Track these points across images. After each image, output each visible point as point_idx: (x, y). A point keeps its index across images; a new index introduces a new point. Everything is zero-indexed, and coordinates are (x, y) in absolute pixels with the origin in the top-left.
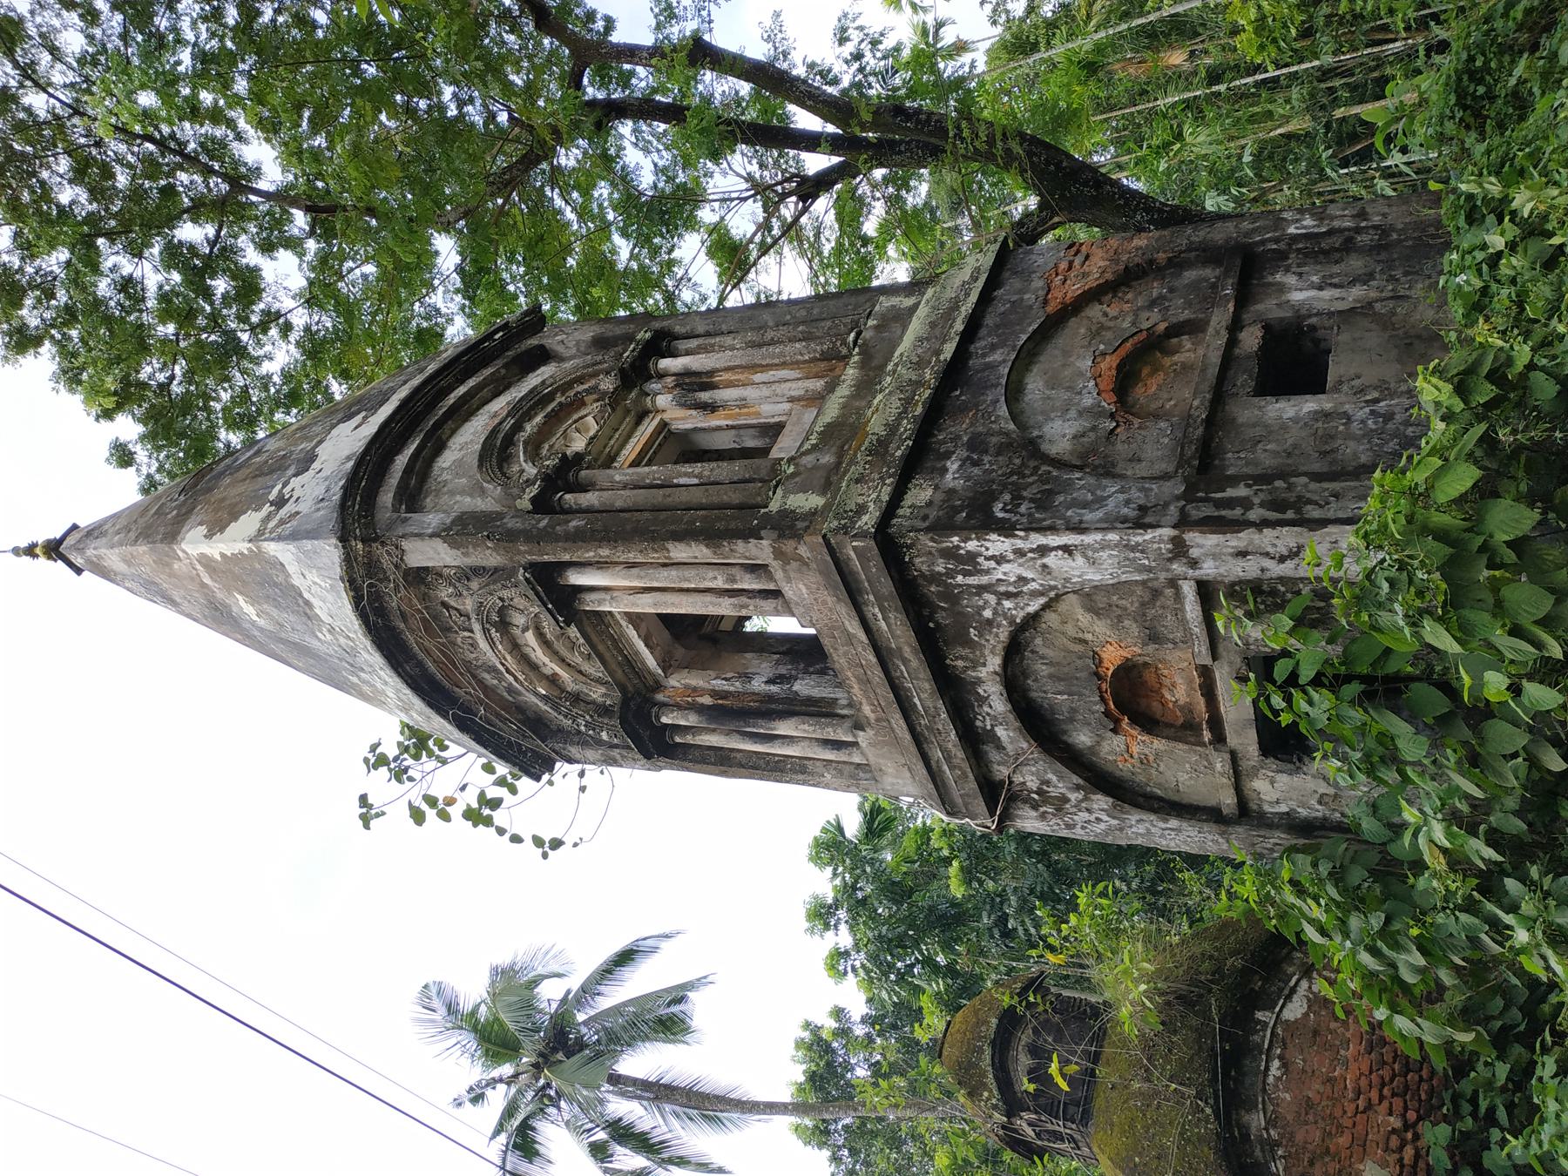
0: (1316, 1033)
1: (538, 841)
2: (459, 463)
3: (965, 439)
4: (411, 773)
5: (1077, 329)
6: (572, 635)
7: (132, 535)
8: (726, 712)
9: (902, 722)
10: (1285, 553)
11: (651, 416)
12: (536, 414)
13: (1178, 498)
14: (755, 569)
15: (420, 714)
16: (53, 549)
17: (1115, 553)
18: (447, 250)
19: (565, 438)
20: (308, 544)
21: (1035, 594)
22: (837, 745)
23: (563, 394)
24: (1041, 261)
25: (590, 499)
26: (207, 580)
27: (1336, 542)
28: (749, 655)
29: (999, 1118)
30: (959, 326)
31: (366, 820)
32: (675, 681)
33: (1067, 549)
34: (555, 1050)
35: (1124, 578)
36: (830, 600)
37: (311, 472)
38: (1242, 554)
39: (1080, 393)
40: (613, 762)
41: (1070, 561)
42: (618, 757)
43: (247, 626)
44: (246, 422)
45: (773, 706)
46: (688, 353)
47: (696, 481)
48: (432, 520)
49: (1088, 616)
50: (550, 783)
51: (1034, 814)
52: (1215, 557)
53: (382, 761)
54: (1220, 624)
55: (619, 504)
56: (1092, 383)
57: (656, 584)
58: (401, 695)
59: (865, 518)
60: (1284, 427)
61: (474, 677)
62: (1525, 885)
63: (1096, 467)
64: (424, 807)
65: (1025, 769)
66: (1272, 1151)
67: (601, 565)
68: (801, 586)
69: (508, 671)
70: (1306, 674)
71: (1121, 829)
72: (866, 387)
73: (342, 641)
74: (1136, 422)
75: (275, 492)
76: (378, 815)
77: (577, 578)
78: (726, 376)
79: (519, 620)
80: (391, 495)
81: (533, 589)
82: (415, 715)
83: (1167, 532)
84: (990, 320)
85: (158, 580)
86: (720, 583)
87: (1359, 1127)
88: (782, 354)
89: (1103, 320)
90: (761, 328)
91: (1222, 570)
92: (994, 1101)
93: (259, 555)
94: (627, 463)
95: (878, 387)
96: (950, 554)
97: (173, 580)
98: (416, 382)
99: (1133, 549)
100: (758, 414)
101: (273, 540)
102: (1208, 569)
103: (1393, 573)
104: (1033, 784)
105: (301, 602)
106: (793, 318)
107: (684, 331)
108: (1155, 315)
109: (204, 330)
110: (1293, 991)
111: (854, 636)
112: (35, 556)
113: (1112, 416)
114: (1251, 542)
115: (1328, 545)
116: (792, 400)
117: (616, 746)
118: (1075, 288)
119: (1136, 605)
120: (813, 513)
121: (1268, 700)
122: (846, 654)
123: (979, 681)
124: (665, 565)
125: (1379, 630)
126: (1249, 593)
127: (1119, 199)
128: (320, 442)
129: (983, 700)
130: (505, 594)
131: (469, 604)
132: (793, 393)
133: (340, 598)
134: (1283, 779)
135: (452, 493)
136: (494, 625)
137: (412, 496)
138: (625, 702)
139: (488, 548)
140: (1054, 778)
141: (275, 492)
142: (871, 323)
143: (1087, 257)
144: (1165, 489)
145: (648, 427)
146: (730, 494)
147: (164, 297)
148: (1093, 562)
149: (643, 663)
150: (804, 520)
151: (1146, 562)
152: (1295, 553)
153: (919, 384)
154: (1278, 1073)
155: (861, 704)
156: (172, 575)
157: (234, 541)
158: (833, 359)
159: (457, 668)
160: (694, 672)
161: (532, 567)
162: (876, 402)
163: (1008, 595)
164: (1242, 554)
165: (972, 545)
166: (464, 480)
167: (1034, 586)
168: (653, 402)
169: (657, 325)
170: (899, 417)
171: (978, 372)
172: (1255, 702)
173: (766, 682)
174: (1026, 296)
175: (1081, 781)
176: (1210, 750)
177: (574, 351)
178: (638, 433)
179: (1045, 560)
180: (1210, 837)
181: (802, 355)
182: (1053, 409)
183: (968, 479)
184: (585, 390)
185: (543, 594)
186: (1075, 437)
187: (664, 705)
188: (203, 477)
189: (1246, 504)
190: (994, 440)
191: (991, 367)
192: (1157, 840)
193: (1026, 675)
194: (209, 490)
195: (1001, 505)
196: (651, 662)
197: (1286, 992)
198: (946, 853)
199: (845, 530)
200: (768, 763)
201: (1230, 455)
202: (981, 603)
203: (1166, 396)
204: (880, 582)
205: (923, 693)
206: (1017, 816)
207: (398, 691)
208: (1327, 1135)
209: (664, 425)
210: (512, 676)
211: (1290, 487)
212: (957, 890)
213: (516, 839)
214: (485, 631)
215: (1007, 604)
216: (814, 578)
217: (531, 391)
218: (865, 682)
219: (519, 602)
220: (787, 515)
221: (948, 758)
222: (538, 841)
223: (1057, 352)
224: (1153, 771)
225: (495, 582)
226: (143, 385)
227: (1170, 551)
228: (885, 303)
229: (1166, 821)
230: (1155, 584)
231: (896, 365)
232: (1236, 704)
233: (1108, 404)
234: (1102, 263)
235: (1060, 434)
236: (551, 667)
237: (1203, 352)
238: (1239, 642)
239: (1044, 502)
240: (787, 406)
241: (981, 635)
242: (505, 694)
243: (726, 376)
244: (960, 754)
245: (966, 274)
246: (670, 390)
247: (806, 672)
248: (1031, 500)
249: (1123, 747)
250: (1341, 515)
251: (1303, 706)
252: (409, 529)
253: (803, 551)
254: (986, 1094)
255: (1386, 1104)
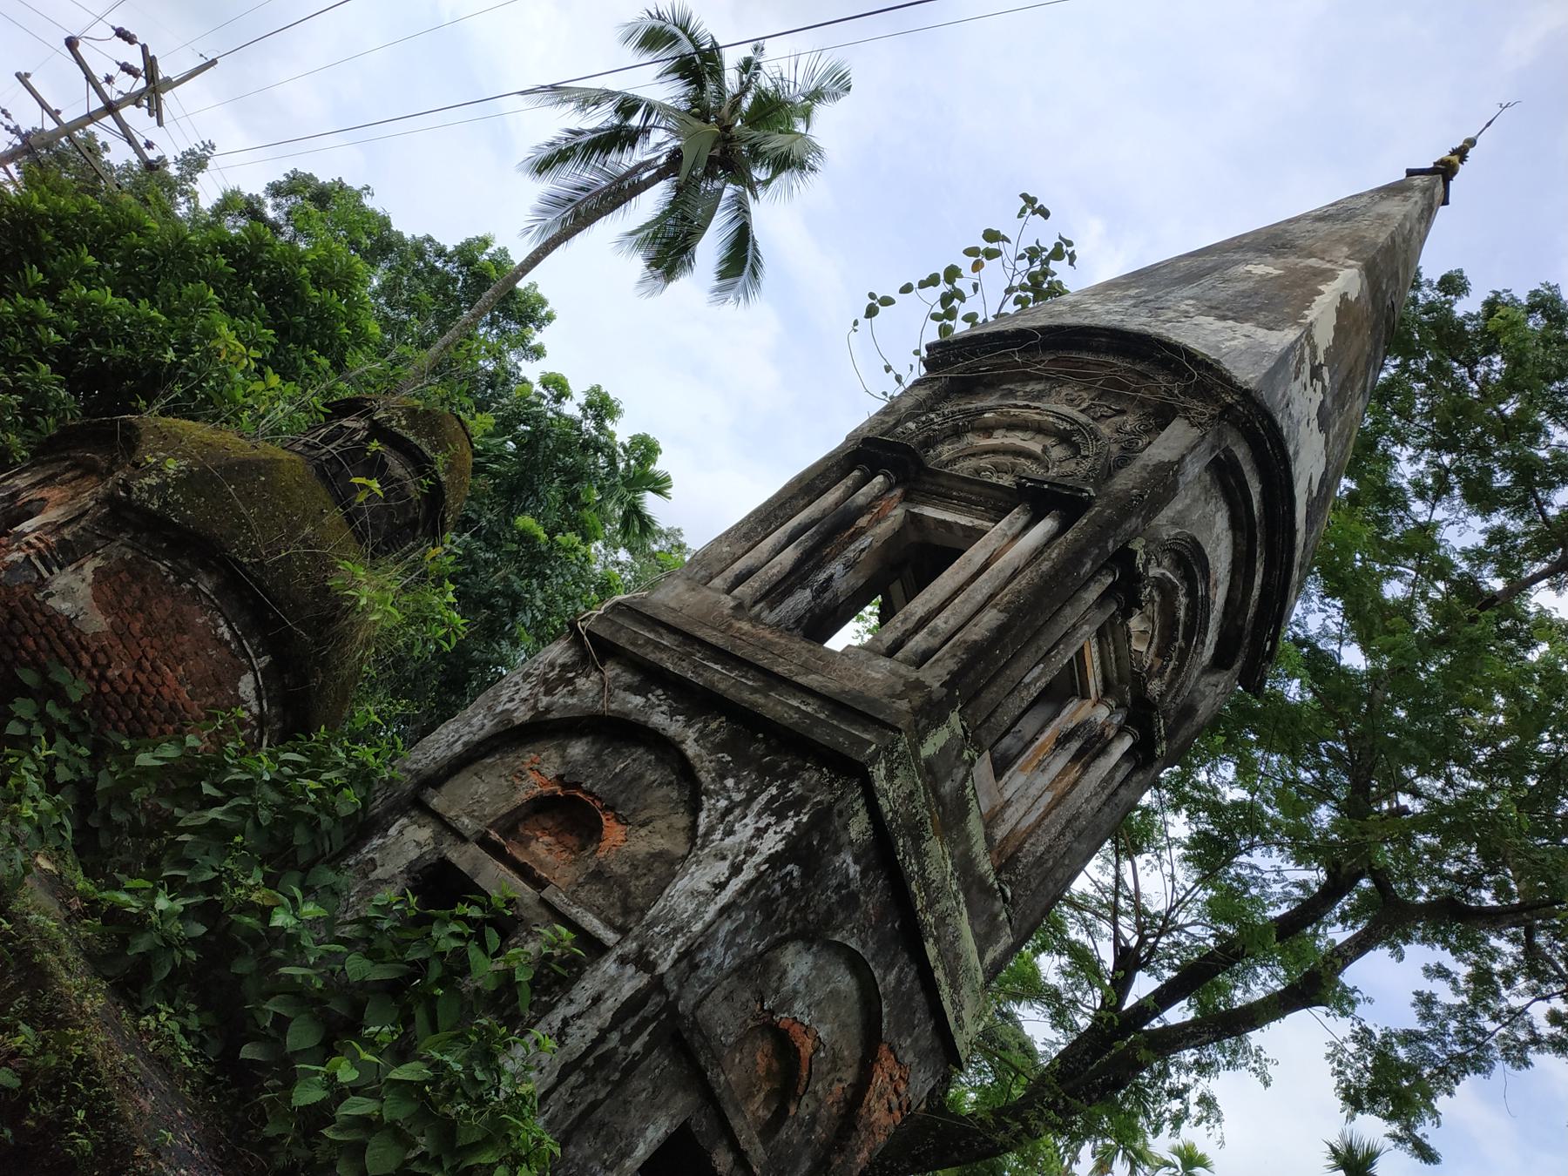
0: (219, 683)
1: (887, 301)
2: (1210, 526)
3: (862, 898)
4: (1026, 262)
5: (850, 1051)
6: (1005, 477)
7: (1399, 240)
8: (840, 526)
9: (713, 641)
10: (568, 1030)
11: (1100, 693)
12: (1186, 615)
13: (678, 998)
14: (923, 658)
15: (1061, 313)
16: (1445, 170)
17: (685, 916)
18: (1353, 657)
19: (1149, 617)
20: (1268, 364)
21: (711, 830)
22: (741, 579)
23: (1180, 648)
24: (921, 1076)
25: (1093, 593)
26: (1312, 262)
27: (541, 1071)
28: (861, 582)
29: (380, 415)
30: (939, 974)
31: (1029, 200)
32: (898, 513)
33: (720, 886)
34: (724, 152)
35: (661, 903)
36: (849, 685)
37: (1314, 415)
38: (597, 1000)
39: (808, 1007)
40: (885, 412)
41: (710, 879)
42: (887, 419)
43: (1250, 255)
44: (1384, 394)
45: (811, 563)
46: (1117, 766)
47: (1027, 680)
48: (1194, 469)
49: (658, 848)
50: (917, 353)
51: (560, 661)
52: (613, 981)
53: (1057, 254)
54: (564, 931)
55: (1068, 611)
56: (807, 1022)
57: (984, 576)
58: (1088, 314)
59: (883, 772)
60: (645, 1119)
61: (1048, 379)
62: (190, 939)
63: (751, 964)
64: (994, 246)
65: (596, 689)
66: (176, 573)
67: (1038, 553)
68: (879, 676)
69: (1028, 407)
70: (474, 953)
71: (489, 708)
72: (965, 866)
73: (1170, 314)
74: (751, 1024)
75: (1326, 376)
76: (1023, 211)
77: (1046, 526)
78: (1073, 775)
79: (1057, 452)
80: (1240, 457)
81: (1071, 488)
82: (1062, 308)
83: (664, 967)
84: (920, 998)
85: (1347, 225)
86: (939, 622)
87: (134, 646)
88: (1047, 831)
89: (839, 1075)
90: (1079, 835)
91: (599, 973)
92: (394, 423)
93: (1295, 319)
94: (1087, 644)
95: (956, 874)
96: (798, 804)
97: (1337, 237)
98: (1298, 555)
99: (675, 931)
100: (1022, 769)
101: (1296, 341)
102: (609, 966)
103: (482, 1090)
104: (581, 682)
105: (1230, 314)
106: (1063, 865)
107: (1134, 779)
108: (804, 1113)
109: (1483, 434)
110: (259, 698)
111: (807, 674)
112: (1454, 152)
113: (772, 1012)
114: (598, 1015)
115: (544, 1063)
116: (1008, 803)
117: (895, 425)
118: (879, 1079)
119: (633, 889)
120: (921, 738)
121: (482, 907)
122: (800, 655)
123: (688, 725)
124: (992, 596)
125: (455, 1038)
126: (565, 973)
127: (891, 1164)
128: (1327, 443)
129: (672, 713)
130: (1087, 464)
131: (1105, 429)
132: (1012, 809)
133: (1205, 346)
134: (414, 854)
135: (1195, 500)
136: (1071, 433)
137: (1224, 473)
138: (920, 465)
139: (1133, 488)
140: (570, 701)
141: (1326, 376)
142: (1003, 916)
143: (890, 1110)
144: (691, 996)
145: (1094, 683)
146: (993, 696)
147: (1538, 429)
148: (694, 894)
149: (934, 506)
150: (924, 728)
151: (657, 930)
152: (561, 1035)
153: (930, 906)
154: (220, 631)
155: (754, 626)
156: (1341, 240)
157: (1322, 312)
158: (1007, 863)
159: (1067, 373)
160: (890, 533)
161: (1087, 504)
162: (949, 862)
163: (728, 811)
164: (597, 1000)
165: (789, 825)
166: (1196, 517)
167: (717, 835)
168: (1109, 706)
169: (1158, 765)
170: (922, 868)
171: (896, 954)
172: (488, 897)
173: (832, 575)
174: (909, 1040)
175: (550, 716)
176: (481, 827)
177: (1201, 687)
178: (1098, 671)
179: (727, 863)
180: (424, 761)
181: (1033, 844)
182: (817, 976)
183: (835, 871)
184: (1167, 666)
185: (1060, 490)
186: (785, 972)
187: (890, 489)
188: (1387, 332)
189: (627, 1040)
190: (841, 917)
191: (888, 968)
192: (457, 725)
193: (659, 760)
194: (1374, 328)
195: (795, 874)
196: (929, 512)
197: (264, 692)
198: (558, 537)
199: (889, 750)
200: (776, 517)
201: (666, 1062)
202: (742, 786)
203: (746, 1061)
204: (828, 735)
205: (719, 677)
206: (570, 648)
207: (1093, 316)
208: (150, 620)
209: (1085, 695)
210: (1018, 404)
211: (606, 1081)
212: (525, 521)
213: (907, 289)
214: (1073, 421)
215: (723, 803)
216: (876, 691)
217: (1206, 628)
218: (766, 647)
219: (1070, 466)
220: (940, 720)
221: (658, 646)
222: (887, 301)
223: (850, 1021)
224: (506, 772)
225: (1103, 466)
226: (1489, 351)
227: (649, 954)
228: (1006, 940)
229: (465, 744)
230: (633, 918)
231: (958, 903)
232: (496, 879)
233: (782, 1018)
234: (876, 1115)
235: (798, 965)
236: (999, 439)
237: (748, 1117)
238: (536, 929)
239: (767, 905)
240: (1007, 795)
241: (719, 761)
242: (1012, 387)
243: (1073, 775)
244: (651, 657)
245: (967, 1015)
246: (1104, 726)
247: (810, 610)
248: (777, 898)
249: (544, 771)
250: (555, 1095)
251: (455, 928)
252: (1204, 446)
253: (903, 705)
254: (404, 423)
255: (130, 679)
